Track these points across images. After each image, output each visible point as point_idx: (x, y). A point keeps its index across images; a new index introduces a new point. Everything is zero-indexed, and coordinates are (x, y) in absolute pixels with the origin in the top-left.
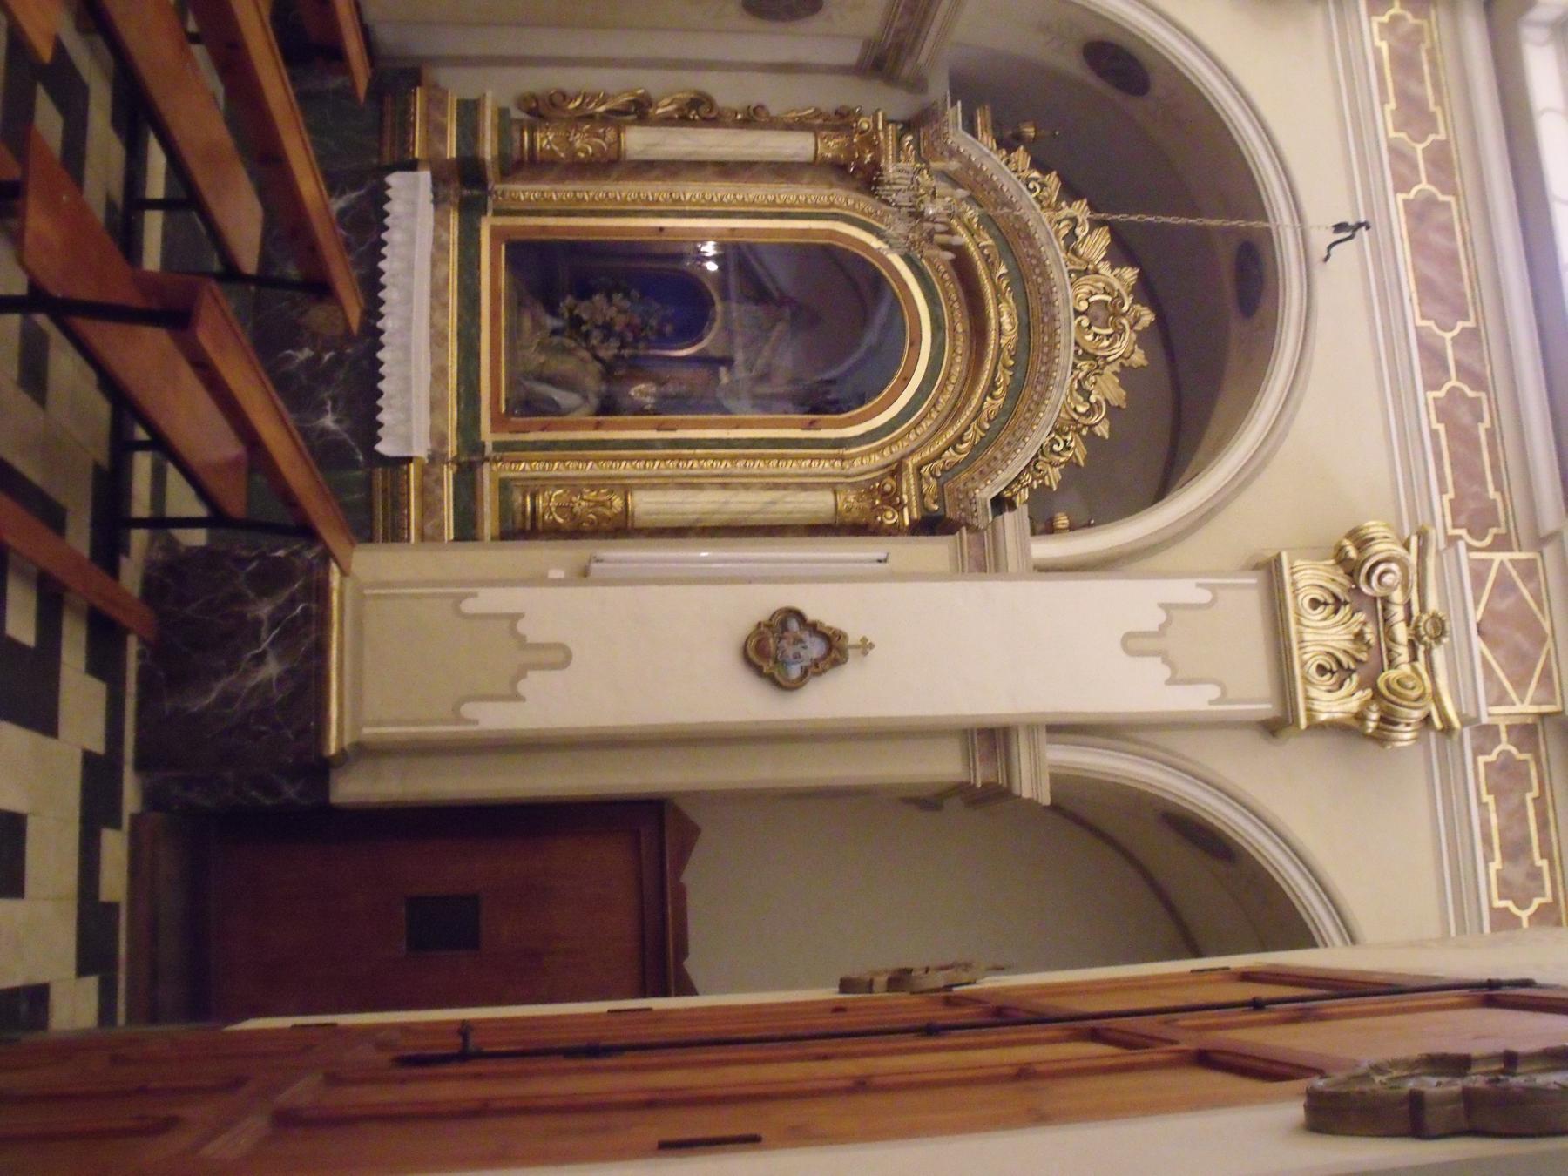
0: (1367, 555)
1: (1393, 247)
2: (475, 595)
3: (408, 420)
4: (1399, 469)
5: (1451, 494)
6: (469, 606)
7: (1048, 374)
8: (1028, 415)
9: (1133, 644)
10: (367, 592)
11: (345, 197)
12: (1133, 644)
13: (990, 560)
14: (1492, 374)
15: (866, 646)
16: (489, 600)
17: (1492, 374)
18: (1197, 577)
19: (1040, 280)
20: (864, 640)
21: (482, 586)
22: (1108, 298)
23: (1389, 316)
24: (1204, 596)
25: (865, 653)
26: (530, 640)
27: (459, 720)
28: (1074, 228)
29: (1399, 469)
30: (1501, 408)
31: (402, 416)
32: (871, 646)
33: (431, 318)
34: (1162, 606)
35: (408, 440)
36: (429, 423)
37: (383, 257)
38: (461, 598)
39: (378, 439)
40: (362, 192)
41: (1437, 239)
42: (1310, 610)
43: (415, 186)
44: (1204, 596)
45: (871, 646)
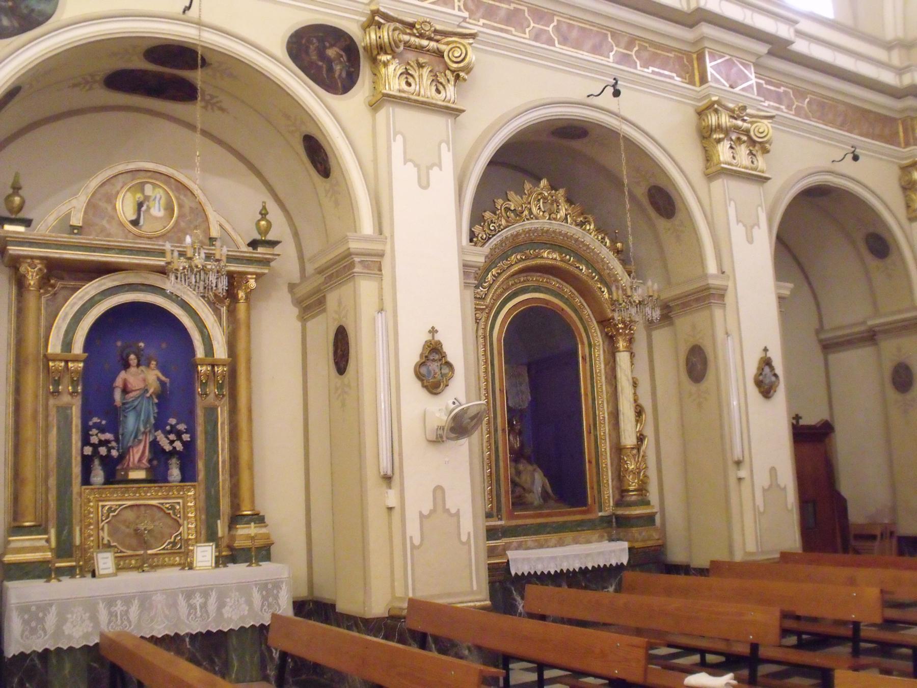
0: (388, 44)
1: (585, 60)
2: (411, 538)
3: (614, 551)
4: (666, 95)
5: (674, 75)
6: (417, 541)
7: (577, 240)
8: (592, 254)
9: (424, 184)
10: (760, 550)
11: (516, 597)
12: (424, 184)
13: (721, 292)
14: (778, 80)
15: (433, 331)
16: (413, 530)
17: (778, 80)
18: (390, 141)
19: (536, 234)
20: (430, 332)
21: (405, 533)
22: (541, 201)
23: (523, 51)
24: (399, 138)
25: (437, 331)
26: (432, 508)
27: (468, 542)
28: (511, 210)
29: (666, 95)
30: (607, 25)
31: (613, 554)
32: (433, 328)
33: (552, 547)
34: (405, 164)
35: (622, 550)
36: (596, 543)
37: (549, 572)
38: (413, 547)
39: (622, 564)
40: (513, 588)
41: (574, 34)
42: (411, 88)
43: (515, 560)
44: (399, 138)
45: (433, 328)
